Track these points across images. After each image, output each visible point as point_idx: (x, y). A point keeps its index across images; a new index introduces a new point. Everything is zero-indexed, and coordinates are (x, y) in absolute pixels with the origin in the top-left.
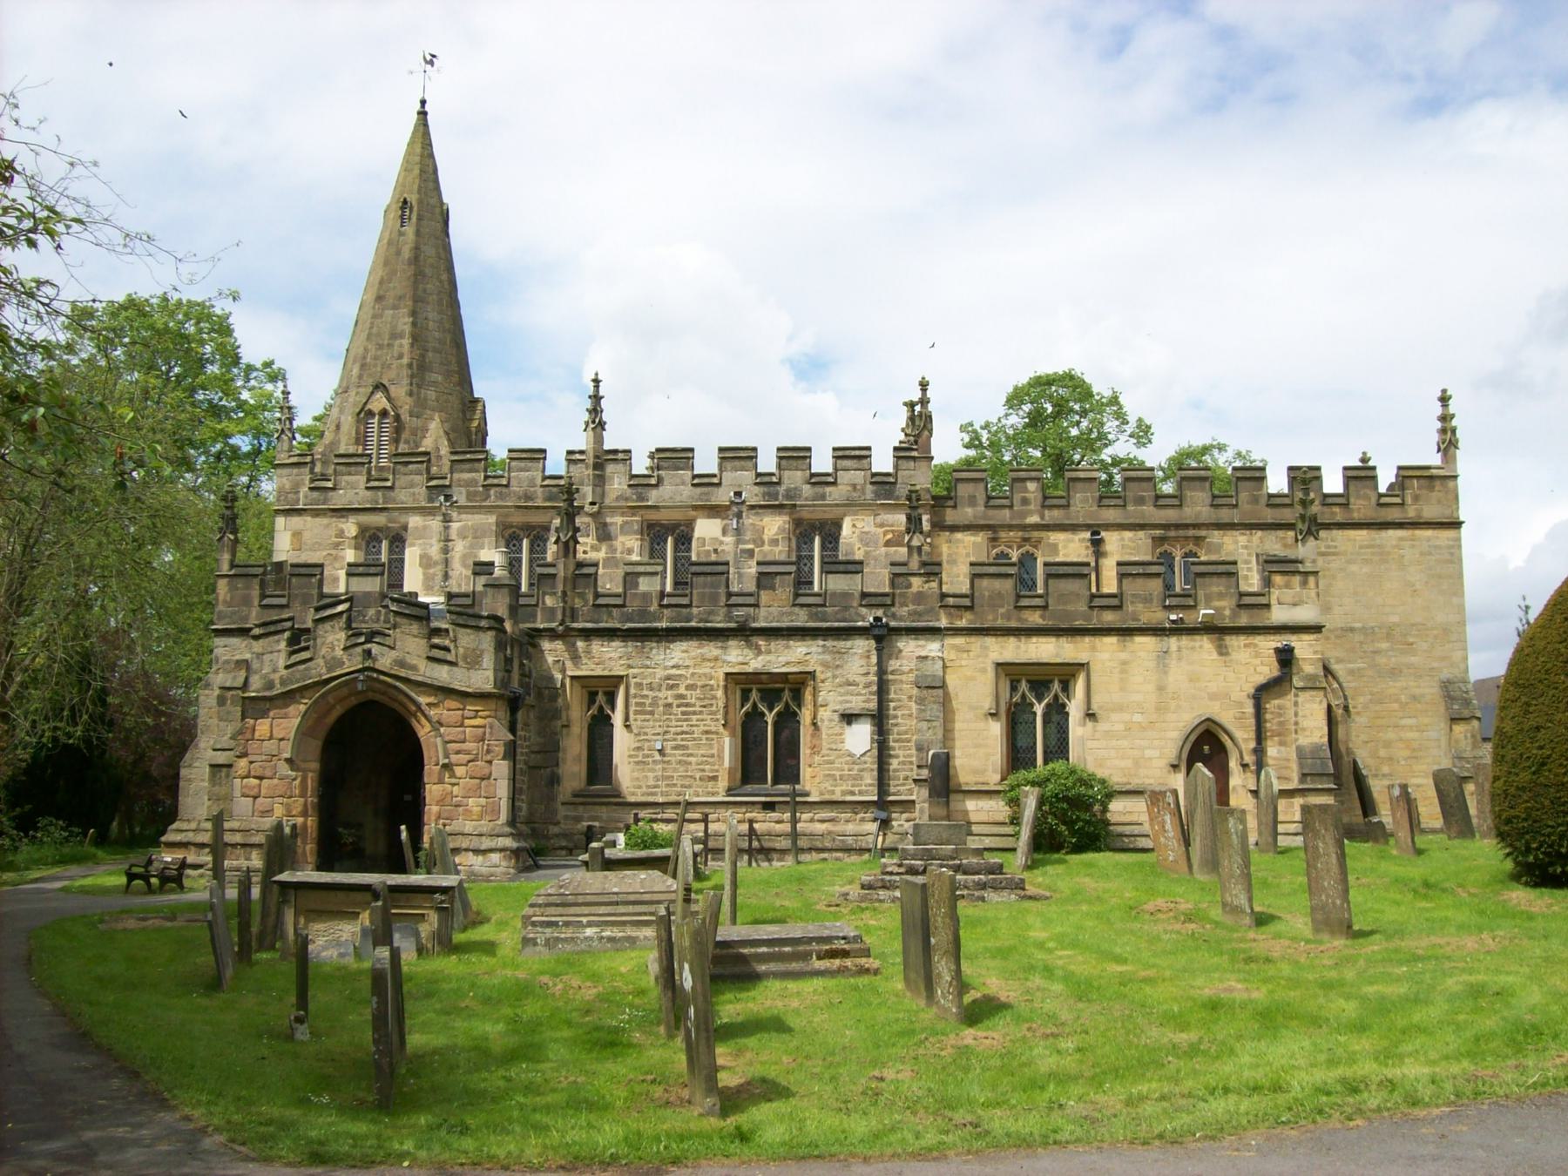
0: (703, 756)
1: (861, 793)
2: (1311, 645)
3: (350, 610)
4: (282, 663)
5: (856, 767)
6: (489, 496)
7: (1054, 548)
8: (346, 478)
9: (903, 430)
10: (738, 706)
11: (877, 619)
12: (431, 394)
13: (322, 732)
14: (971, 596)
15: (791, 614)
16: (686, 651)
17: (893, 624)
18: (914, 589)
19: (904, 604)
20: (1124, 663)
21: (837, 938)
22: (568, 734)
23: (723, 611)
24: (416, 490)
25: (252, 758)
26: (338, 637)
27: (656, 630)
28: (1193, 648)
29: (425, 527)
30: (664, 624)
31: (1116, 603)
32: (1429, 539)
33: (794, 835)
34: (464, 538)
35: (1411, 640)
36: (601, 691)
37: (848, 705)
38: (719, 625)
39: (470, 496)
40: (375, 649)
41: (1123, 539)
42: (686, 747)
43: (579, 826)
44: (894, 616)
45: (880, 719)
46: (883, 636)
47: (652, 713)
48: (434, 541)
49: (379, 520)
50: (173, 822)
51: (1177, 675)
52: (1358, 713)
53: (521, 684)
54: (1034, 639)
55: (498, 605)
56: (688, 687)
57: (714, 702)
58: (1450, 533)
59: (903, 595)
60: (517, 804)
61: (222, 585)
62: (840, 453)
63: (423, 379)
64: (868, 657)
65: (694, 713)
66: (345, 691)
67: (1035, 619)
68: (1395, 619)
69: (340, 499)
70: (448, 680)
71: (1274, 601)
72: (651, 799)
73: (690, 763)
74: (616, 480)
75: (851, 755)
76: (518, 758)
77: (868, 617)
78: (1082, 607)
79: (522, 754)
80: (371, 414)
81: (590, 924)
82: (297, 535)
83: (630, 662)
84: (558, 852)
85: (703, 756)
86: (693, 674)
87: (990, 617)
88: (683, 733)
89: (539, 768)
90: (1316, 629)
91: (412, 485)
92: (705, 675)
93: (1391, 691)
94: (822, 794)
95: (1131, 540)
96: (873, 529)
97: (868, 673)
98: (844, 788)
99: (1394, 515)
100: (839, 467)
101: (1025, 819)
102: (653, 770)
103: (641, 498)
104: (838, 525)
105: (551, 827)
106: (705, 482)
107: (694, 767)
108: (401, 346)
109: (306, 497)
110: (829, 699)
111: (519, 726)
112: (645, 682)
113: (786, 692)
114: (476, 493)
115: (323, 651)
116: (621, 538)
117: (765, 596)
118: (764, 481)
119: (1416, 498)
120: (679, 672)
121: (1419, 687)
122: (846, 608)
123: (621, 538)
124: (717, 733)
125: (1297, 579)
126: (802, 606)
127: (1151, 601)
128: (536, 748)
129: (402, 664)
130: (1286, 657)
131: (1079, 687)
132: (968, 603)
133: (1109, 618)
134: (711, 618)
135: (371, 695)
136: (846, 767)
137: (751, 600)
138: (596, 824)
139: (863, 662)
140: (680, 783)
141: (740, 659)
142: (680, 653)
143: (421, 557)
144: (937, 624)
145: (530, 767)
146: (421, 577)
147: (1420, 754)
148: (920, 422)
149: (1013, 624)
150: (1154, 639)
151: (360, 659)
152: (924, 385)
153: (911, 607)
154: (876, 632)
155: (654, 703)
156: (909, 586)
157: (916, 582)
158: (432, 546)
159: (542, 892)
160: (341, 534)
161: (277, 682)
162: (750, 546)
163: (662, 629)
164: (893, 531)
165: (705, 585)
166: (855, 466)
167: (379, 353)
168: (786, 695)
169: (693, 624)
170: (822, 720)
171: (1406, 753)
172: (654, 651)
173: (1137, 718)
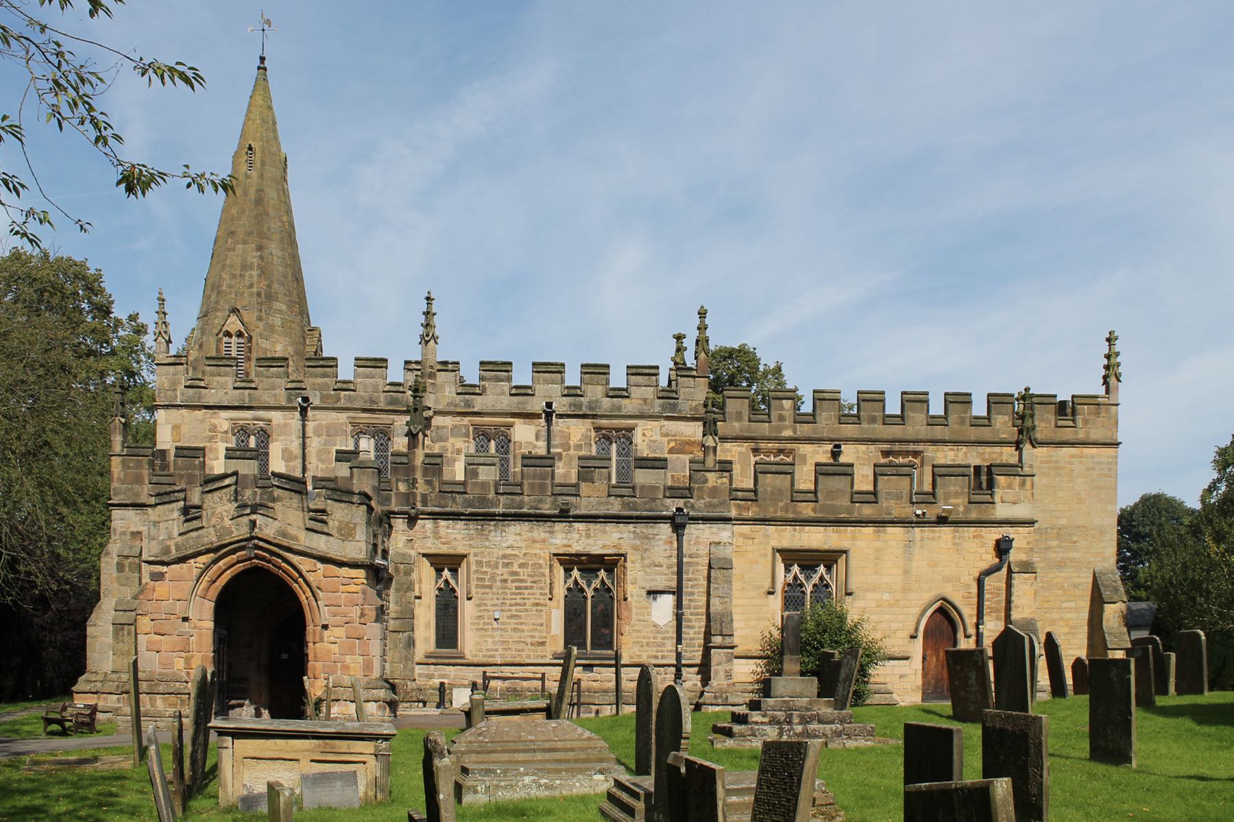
1: (663, 657)
2: (1025, 537)
3: (236, 483)
4: (175, 533)
5: (660, 636)
6: (339, 399)
8: (217, 378)
11: (679, 509)
12: (277, 321)
14: (755, 491)
15: (607, 503)
17: (691, 513)
18: (710, 484)
19: (700, 498)
20: (878, 550)
23: (549, 499)
26: (226, 508)
27: (494, 515)
28: (933, 539)
29: (285, 425)
30: (500, 510)
32: (1093, 457)
34: (319, 436)
35: (1075, 539)
36: (446, 563)
37: (656, 583)
39: (323, 398)
41: (858, 452)
43: (431, 683)
44: (692, 507)
45: (678, 592)
46: (678, 524)
47: (490, 587)
48: (294, 437)
50: (83, 673)
51: (919, 562)
55: (364, 483)
56: (521, 566)
57: (542, 578)
58: (1109, 451)
59: (700, 489)
61: (116, 461)
62: (634, 371)
63: (270, 307)
64: (671, 543)
65: (526, 588)
67: (807, 510)
68: (1063, 522)
69: (211, 397)
70: (325, 550)
71: (997, 498)
72: (491, 660)
73: (523, 631)
74: (447, 389)
77: (672, 506)
78: (846, 502)
80: (228, 334)
82: (176, 428)
83: (471, 542)
85: (533, 624)
86: (525, 554)
87: (771, 510)
88: (516, 604)
90: (1031, 523)
91: (273, 388)
92: (535, 555)
93: (1056, 580)
95: (864, 453)
96: (659, 438)
97: (671, 556)
98: (650, 653)
100: (632, 382)
102: (493, 636)
106: (522, 391)
107: (526, 634)
108: (251, 276)
109: (182, 394)
112: (484, 560)
114: (328, 396)
116: (451, 440)
117: (585, 488)
118: (571, 392)
119: (1086, 422)
120: (513, 552)
121: (1079, 577)
122: (654, 500)
123: (451, 440)
126: (617, 496)
127: (901, 498)
129: (284, 534)
130: (1002, 548)
132: (753, 495)
133: (867, 511)
136: (651, 635)
139: (667, 547)
140: (514, 647)
141: (565, 542)
142: (514, 536)
143: (284, 451)
144: (726, 514)
147: (1076, 631)
149: (791, 516)
153: (707, 500)
155: (493, 578)
156: (706, 481)
158: (292, 442)
160: (213, 428)
161: (173, 548)
164: (675, 440)
165: (535, 476)
166: (646, 383)
167: (233, 282)
169: (525, 510)
170: (632, 596)
171: (1066, 630)
172: (493, 534)
173: (886, 596)
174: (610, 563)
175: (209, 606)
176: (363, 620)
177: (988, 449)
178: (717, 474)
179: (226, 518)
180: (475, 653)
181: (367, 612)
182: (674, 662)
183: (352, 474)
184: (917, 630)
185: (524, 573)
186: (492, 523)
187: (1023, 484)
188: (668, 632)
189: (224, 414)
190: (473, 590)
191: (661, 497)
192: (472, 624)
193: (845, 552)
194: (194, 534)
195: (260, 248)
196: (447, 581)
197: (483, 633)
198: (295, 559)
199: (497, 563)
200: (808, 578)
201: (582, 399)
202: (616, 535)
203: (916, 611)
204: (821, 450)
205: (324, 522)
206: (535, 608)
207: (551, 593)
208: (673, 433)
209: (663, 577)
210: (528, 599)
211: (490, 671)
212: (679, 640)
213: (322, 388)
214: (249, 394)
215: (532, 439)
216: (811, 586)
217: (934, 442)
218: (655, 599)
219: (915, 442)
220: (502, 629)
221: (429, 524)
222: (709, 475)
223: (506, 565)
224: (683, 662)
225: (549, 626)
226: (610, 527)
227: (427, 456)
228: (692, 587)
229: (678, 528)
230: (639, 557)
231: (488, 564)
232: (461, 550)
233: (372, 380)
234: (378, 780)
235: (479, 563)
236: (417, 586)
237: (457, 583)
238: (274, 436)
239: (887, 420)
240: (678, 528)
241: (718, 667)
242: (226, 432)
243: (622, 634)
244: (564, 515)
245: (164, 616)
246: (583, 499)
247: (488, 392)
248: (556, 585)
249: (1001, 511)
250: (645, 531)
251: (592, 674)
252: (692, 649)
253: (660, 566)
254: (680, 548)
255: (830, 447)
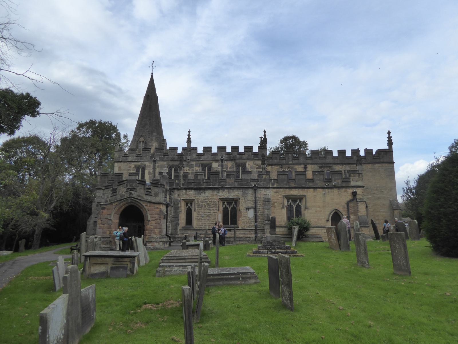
0: (213, 218)
1: (251, 227)
7: (296, 169)
9: (260, 143)
10: (222, 206)
13: (119, 213)
16: (209, 193)
17: (258, 186)
19: (261, 182)
21: (248, 273)
22: (181, 213)
24: (148, 157)
25: (101, 219)
27: (202, 188)
28: (332, 192)
29: (149, 165)
31: (312, 181)
33: (235, 237)
35: (382, 191)
36: (189, 202)
37: (248, 206)
38: (217, 187)
40: (132, 192)
41: (312, 167)
42: (209, 216)
44: (259, 184)
45: (255, 209)
46: (255, 189)
47: (201, 208)
49: (139, 164)
52: (370, 208)
53: (169, 201)
54: (293, 190)
56: (210, 202)
60: (168, 230)
64: (253, 194)
65: (211, 208)
66: (125, 203)
67: (293, 185)
71: (351, 180)
72: (201, 229)
73: (210, 220)
75: (249, 218)
76: (168, 219)
79: (170, 218)
80: (140, 142)
81: (176, 266)
82: (120, 167)
83: (196, 196)
84: (178, 242)
86: (211, 199)
88: (208, 213)
89: (174, 221)
90: (363, 187)
91: (146, 156)
92: (214, 199)
94: (242, 227)
96: (253, 165)
97: (253, 198)
99: (378, 161)
101: (295, 234)
102: (202, 222)
103: (200, 158)
104: (245, 164)
105: (176, 236)
107: (211, 221)
110: (243, 205)
111: (169, 211)
113: (233, 202)
115: (120, 193)
116: (195, 168)
120: (208, 198)
122: (248, 183)
123: (195, 168)
124: (216, 213)
125: (357, 175)
126: (237, 182)
128: (173, 216)
129: (139, 196)
130: (354, 194)
131: (304, 200)
132: (276, 181)
133: (311, 184)
134: (216, 185)
135: (131, 203)
136: (248, 221)
137: (224, 181)
138: (188, 235)
139: (252, 195)
141: (222, 195)
142: (208, 194)
144: (268, 186)
145: (172, 221)
146: (148, 177)
148: (264, 142)
149: (288, 186)
150: (322, 189)
151: (129, 195)
152: (265, 132)
154: (254, 188)
156: (263, 177)
157: (264, 176)
159: (165, 256)
160: (130, 167)
161: (108, 201)
162: (225, 169)
163: (204, 188)
168: (233, 203)
169: (211, 187)
170: (242, 209)
174: (236, 201)
175: (118, 216)
176: (160, 219)
177: (352, 165)
178: (266, 175)
179: (123, 192)
180: (196, 226)
181: (161, 216)
182: (255, 228)
183: (161, 178)
184: (328, 219)
185: (211, 204)
186: (202, 190)
187: (359, 176)
188: (252, 220)
189: (133, 163)
190: (196, 209)
191: (250, 182)
192: (196, 218)
193: (305, 196)
194: (114, 197)
195: (150, 120)
196: (189, 207)
197: (198, 221)
198: (142, 203)
199: (203, 201)
200: (294, 204)
201: (231, 156)
202: (237, 193)
203: (328, 213)
204: (301, 167)
205: (150, 192)
206: (213, 214)
207: (218, 209)
208: (257, 164)
209: (251, 204)
210: (212, 211)
211: (199, 232)
212: (256, 222)
213: (160, 155)
214: (140, 158)
215: (217, 166)
216: (295, 206)
217: (335, 164)
218: (248, 210)
219: (329, 164)
220: (204, 220)
221: (184, 191)
222: (263, 175)
223: (205, 202)
224: (257, 228)
225: (218, 218)
226: (235, 191)
227: (184, 173)
228: (259, 207)
229: (255, 190)
230: (244, 198)
231: (201, 202)
232: (193, 198)
233: (173, 153)
234: (131, 269)
235: (198, 201)
236: (180, 208)
237: (192, 207)
238: (146, 168)
239: (320, 158)
240: (255, 190)
241: (267, 230)
242: (133, 168)
243: (239, 221)
244: (223, 188)
245: (104, 219)
246: (228, 183)
247: (205, 155)
248: (220, 207)
249: (353, 184)
250: (245, 191)
251: (230, 232)
252: (260, 224)
253: (250, 201)
254: (255, 196)
255: (303, 166)
